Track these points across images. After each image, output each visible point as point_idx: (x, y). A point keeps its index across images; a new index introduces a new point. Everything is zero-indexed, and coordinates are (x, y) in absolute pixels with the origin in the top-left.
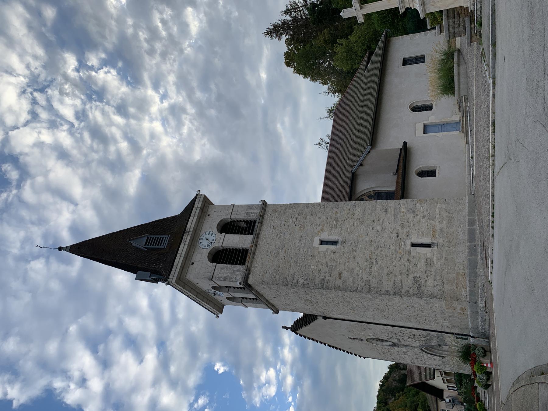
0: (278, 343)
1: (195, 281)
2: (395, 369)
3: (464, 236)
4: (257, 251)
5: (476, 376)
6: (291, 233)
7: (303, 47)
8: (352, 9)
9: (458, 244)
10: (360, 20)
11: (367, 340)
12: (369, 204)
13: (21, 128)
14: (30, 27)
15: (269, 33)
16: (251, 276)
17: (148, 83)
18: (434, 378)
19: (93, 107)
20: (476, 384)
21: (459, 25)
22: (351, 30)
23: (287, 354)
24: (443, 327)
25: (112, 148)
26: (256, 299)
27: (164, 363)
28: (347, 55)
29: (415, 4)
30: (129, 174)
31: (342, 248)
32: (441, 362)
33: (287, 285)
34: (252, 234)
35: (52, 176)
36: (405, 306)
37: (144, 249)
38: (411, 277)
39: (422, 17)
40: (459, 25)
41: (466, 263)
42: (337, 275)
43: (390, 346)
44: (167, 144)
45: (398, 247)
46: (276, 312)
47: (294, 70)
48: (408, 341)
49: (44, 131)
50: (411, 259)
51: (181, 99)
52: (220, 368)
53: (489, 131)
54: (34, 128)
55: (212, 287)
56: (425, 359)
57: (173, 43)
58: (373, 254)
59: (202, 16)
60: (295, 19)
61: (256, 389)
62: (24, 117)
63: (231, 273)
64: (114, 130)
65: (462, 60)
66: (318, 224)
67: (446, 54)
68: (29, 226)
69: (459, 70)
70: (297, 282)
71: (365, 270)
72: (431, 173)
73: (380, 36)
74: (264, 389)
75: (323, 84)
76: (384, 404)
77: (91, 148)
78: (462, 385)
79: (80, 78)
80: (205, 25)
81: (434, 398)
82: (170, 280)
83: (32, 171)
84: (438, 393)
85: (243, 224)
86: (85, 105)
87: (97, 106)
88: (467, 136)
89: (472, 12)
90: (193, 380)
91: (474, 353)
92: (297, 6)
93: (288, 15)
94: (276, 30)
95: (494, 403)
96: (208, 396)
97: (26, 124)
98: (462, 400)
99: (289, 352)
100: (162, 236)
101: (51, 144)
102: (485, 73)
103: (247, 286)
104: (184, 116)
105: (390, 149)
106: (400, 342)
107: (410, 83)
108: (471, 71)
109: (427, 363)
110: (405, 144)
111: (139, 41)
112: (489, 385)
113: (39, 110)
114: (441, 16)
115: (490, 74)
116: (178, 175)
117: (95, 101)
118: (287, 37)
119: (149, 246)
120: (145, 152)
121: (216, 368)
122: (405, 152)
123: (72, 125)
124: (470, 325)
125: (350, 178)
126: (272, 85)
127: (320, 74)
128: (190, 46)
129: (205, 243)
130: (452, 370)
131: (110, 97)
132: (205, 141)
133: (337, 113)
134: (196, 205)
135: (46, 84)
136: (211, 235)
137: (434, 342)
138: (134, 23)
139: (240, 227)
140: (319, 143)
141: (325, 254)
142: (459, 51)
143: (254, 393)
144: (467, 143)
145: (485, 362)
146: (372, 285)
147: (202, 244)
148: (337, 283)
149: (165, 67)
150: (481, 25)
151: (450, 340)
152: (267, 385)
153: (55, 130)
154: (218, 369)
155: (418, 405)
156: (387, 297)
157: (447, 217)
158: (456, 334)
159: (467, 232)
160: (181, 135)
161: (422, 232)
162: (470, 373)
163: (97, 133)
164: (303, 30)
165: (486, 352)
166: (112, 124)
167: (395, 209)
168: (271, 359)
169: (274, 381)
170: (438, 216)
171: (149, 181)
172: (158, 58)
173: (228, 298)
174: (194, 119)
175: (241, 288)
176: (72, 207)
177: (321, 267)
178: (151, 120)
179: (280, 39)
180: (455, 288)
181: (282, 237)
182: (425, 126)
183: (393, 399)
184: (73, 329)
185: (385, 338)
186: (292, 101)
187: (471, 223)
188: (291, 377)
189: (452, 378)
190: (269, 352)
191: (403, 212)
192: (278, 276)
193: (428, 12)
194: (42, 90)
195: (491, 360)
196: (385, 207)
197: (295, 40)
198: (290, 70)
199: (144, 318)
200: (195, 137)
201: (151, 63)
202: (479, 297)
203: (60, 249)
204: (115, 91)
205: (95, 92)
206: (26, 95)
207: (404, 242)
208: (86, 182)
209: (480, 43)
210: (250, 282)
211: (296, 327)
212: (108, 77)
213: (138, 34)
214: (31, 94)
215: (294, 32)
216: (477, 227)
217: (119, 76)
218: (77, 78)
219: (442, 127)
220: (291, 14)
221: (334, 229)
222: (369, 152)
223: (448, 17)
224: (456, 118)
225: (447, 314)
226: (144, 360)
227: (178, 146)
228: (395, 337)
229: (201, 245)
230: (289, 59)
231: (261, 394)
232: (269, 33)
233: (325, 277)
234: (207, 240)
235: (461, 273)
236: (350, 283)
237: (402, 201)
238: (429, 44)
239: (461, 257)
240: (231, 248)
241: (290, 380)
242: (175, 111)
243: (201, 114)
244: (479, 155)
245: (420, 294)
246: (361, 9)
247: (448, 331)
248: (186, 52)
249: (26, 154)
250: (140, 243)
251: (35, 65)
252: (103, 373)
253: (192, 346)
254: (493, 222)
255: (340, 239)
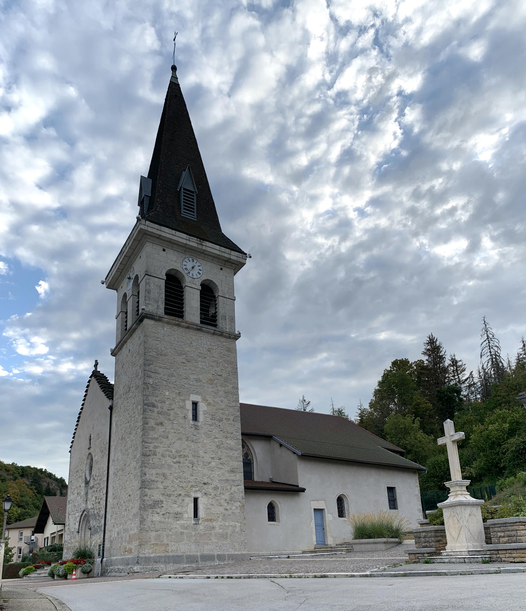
0: (78, 356)
1: (143, 254)
2: (60, 484)
3: (207, 550)
4: (181, 329)
5: (62, 564)
6: (204, 369)
7: (413, 381)
8: (452, 432)
9: (198, 545)
10: (440, 441)
11: (90, 454)
12: (238, 454)
13: (327, 11)
14: (459, 23)
15: (432, 341)
16: (152, 322)
17: (379, 192)
18: (55, 524)
19: (352, 116)
20: (53, 565)
21: (428, 542)
22: (431, 432)
23: (66, 367)
24: (110, 531)
25: (300, 144)
26: (126, 329)
27: (41, 217)
28: (402, 428)
29: (453, 497)
30: (268, 168)
31: (190, 426)
32: (73, 530)
33: (144, 365)
34: (201, 322)
35: (266, 58)
36: (131, 493)
37: (178, 188)
38: (162, 498)
39: (438, 505)
40: (428, 542)
41: (179, 554)
42: (159, 421)
43: (86, 478)
44: (305, 218)
45: (194, 484)
46: (114, 353)
47: (388, 371)
48: (92, 496)
49: (324, 44)
50: (181, 498)
51: (358, 234)
52: (43, 287)
53: (317, 572)
54: (328, 30)
55: (137, 275)
56: (75, 514)
57: (426, 224)
58: (185, 459)
59: (457, 259)
60: (445, 370)
61: (23, 332)
62: (343, 16)
63: (155, 299)
64: (323, 146)
65: (391, 545)
66: (216, 400)
67: (397, 531)
68: (200, 25)
69: (381, 543)
70: (149, 377)
71: (167, 450)
72: (272, 517)
73: (420, 463)
74: (23, 340)
75: (370, 403)
76: (21, 473)
77: (300, 115)
78: (51, 551)
79: (390, 97)
80: (446, 263)
81: (34, 524)
82: (143, 221)
83: (272, 29)
84: (40, 528)
85: (212, 311)
86: (355, 105)
87: (353, 121)
88: (311, 552)
89: (440, 554)
90: (24, 253)
91: (85, 563)
92: (459, 372)
93: (450, 362)
94: (434, 349)
95: (35, 582)
96: (8, 273)
97: (333, 18)
98: (35, 552)
99: (69, 369)
100: (195, 211)
101: (306, 56)
102: (376, 567)
103: (141, 318)
104: (337, 238)
105: (297, 476)
106: (91, 489)
107: (367, 495)
108: (380, 554)
109: (70, 516)
110: (303, 490)
111: (431, 180)
112: (53, 577)
113: (351, 38)
114: (438, 524)
115: (375, 572)
116: (268, 232)
117: (360, 119)
118: (426, 362)
119: (182, 194)
120: (295, 188)
121: (41, 282)
122: (295, 490)
123: (330, 87)
124: (115, 558)
125: (266, 434)
126: (370, 346)
127: (382, 400)
128: (422, 245)
129: (189, 265)
130: (65, 541)
131: (363, 140)
132: (308, 265)
133: (338, 419)
134: (233, 253)
135: (384, 48)
136: (198, 273)
137: (93, 523)
138: (454, 171)
139: (209, 307)
140: (305, 401)
141: (183, 407)
142: (400, 543)
143: (18, 329)
144: (304, 552)
145: (77, 573)
146: (151, 458)
147: (187, 261)
148: (152, 420)
149: (397, 214)
150: (427, 562)
151: (97, 539)
152: (29, 344)
153: (325, 62)
154: (40, 285)
155: (25, 509)
156: (139, 474)
157: (227, 533)
158: (104, 544)
159: (211, 553)
160: (315, 235)
161: (210, 509)
162: (64, 559)
163: (320, 122)
164: (433, 380)
165: (88, 574)
166: (330, 143)
167: (234, 481)
168: (58, 348)
169: (34, 352)
170: (227, 524)
171: (259, 195)
172: (408, 203)
173: (125, 295)
174: (333, 252)
175: (138, 310)
176: (226, 88)
177: (167, 403)
178: (334, 197)
179: (424, 353)
180: (152, 543)
181: (200, 359)
182: (321, 510)
183: (28, 483)
184: (72, 91)
185: (93, 473)
186: (354, 369)
187: (221, 557)
188: (42, 372)
189: (56, 541)
190: (66, 346)
191: (231, 489)
192: (154, 354)
193: (444, 510)
194: (377, 42)
195: (80, 578)
196: (236, 470)
197: (423, 371)
198: (388, 366)
199: (93, 189)
200: (312, 252)
201: (404, 195)
202: (143, 566)
203: (174, 68)
204: (371, 147)
205: (371, 119)
206: (371, 18)
207: (199, 490)
208: (258, 108)
209: (407, 562)
210: (146, 321)
211: (98, 377)
212: (388, 138)
213: (440, 177)
214: (373, 26)
215: (431, 369)
216: (217, 563)
217: (389, 152)
218: (389, 93)
219: (321, 527)
220: (451, 366)
221: (210, 417)
222: (294, 453)
223: (436, 531)
224: (330, 541)
225: (124, 535)
226: (42, 191)
227: (302, 231)
228: (95, 483)
229: (187, 260)
230: (400, 365)
231: (17, 337)
232: (432, 341)
233: (156, 407)
234: (193, 268)
235: (167, 548)
236: (152, 434)
237: (242, 487)
238: (410, 513)
239: (185, 548)
240: (184, 297)
241: (37, 370)
242: (343, 227)
243: (339, 260)
244: (291, 564)
245: (143, 507)
246: (452, 441)
247: (106, 537)
248: (414, 240)
249: (294, 19)
250: (186, 182)
251: (408, 32)
252: (20, 135)
253: (65, 253)
254: (223, 578)
255: (199, 424)
